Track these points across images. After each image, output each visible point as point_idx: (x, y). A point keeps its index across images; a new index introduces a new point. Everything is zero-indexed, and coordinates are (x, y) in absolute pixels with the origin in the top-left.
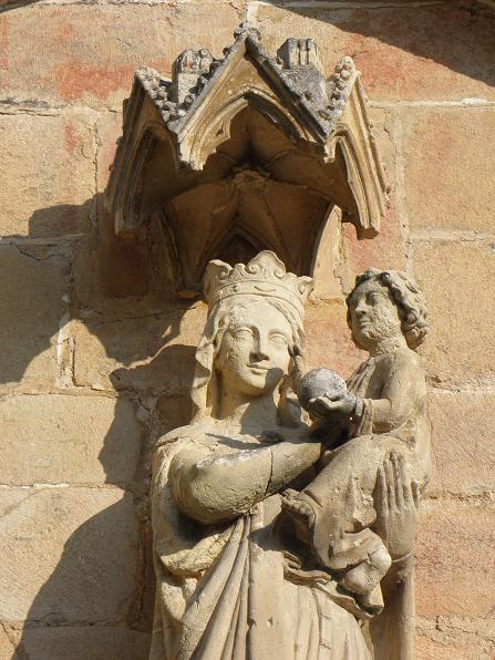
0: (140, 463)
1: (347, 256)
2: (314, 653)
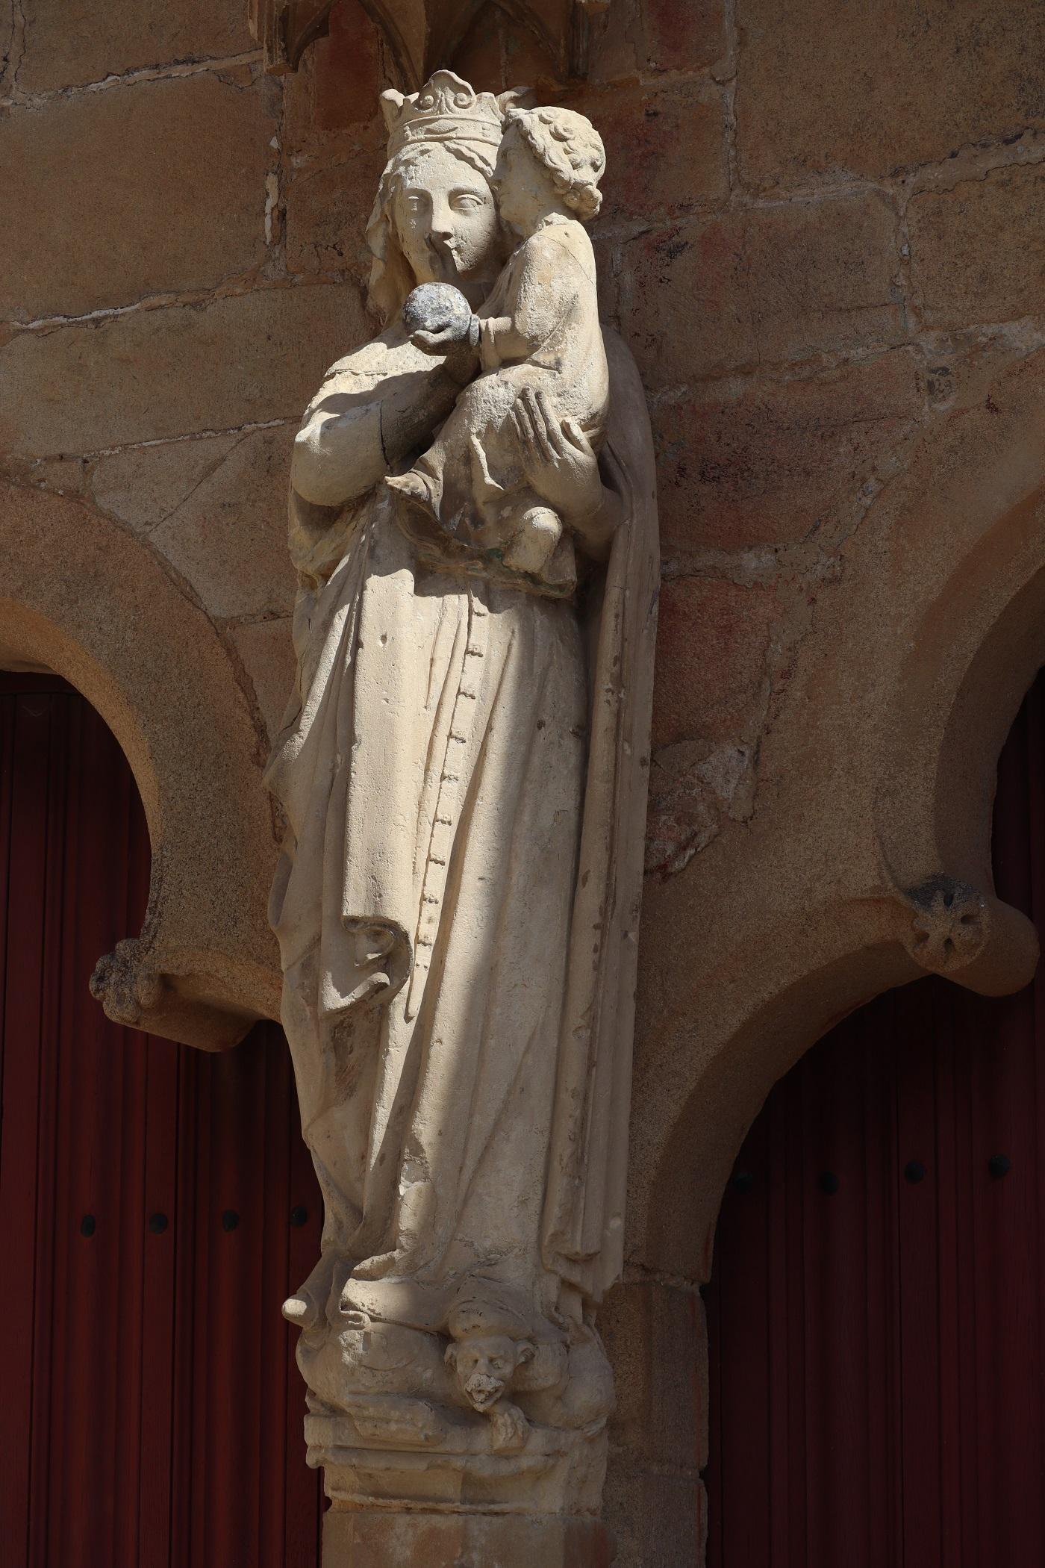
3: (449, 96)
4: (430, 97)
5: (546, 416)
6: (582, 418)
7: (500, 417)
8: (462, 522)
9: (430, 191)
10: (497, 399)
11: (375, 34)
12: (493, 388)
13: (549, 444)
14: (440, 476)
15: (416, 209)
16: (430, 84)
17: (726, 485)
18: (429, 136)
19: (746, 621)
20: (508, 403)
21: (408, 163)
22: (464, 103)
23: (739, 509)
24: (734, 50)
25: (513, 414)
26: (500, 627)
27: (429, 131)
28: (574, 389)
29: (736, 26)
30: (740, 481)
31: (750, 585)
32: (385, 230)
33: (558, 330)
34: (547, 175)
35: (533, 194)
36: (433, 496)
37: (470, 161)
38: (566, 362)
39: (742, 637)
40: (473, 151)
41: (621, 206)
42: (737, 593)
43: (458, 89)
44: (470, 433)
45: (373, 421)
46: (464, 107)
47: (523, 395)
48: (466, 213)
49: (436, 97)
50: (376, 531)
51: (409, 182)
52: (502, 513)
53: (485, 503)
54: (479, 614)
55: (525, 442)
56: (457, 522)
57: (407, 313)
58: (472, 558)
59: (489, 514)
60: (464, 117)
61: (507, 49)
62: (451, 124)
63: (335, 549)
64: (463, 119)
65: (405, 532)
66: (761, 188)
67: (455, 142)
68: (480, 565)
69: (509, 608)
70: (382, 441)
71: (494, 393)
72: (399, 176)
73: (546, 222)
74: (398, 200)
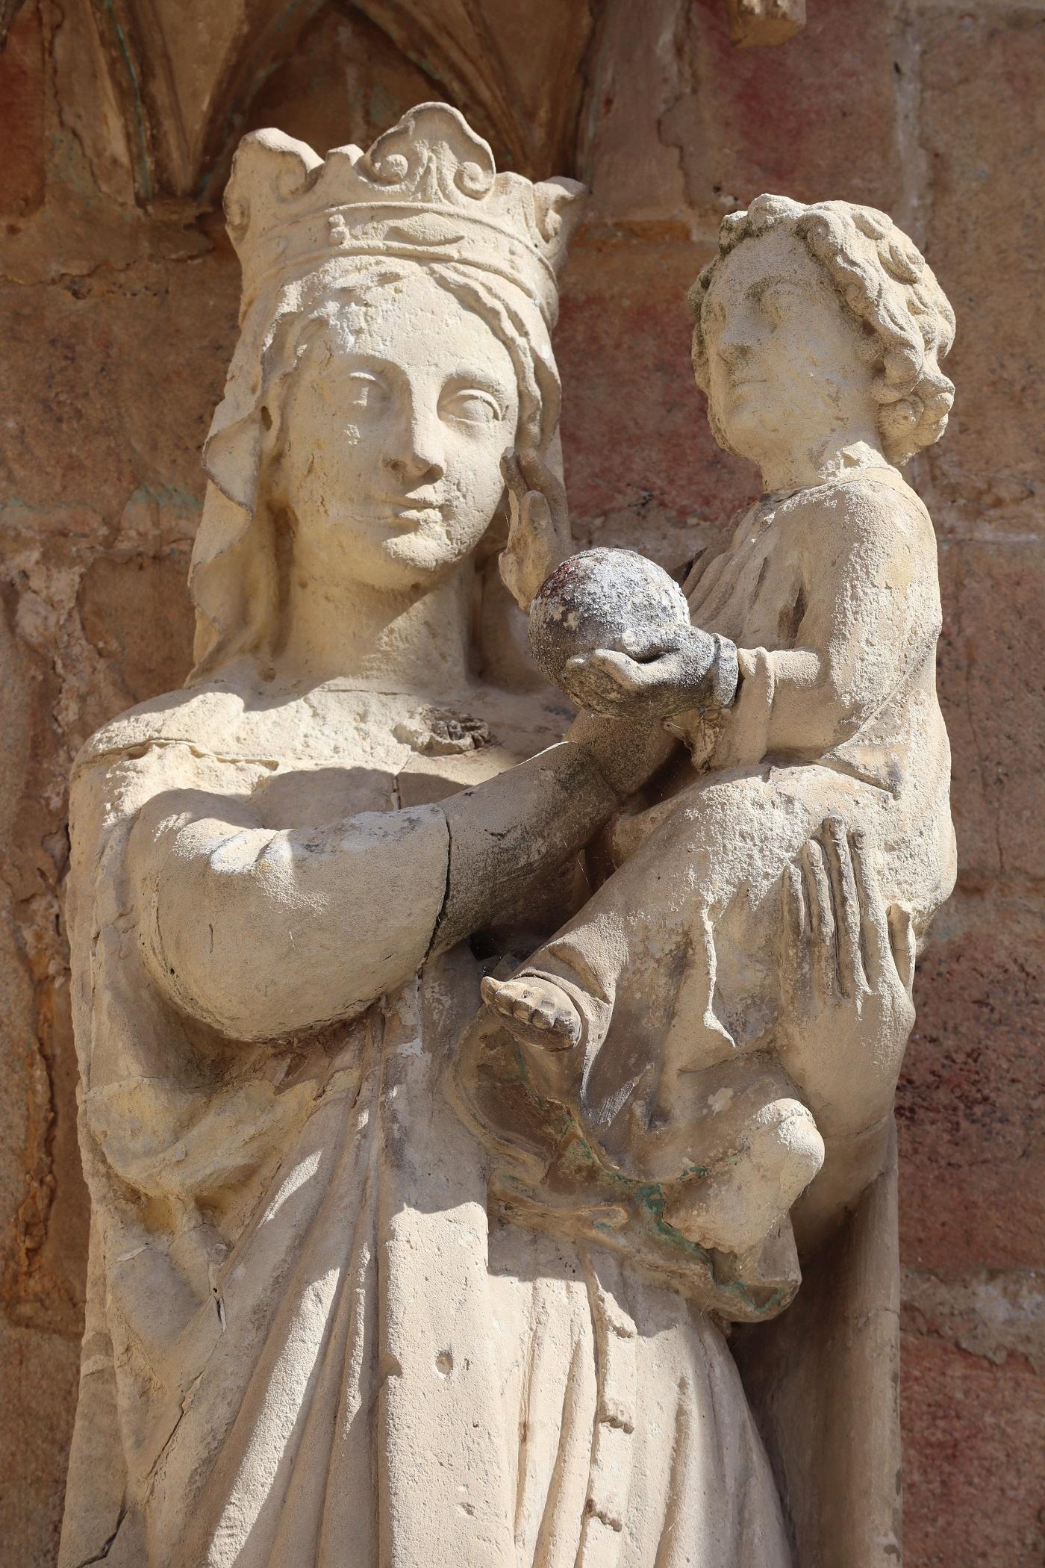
0: (33, 787)
1: (703, 70)
2: (581, 1445)
3: (447, 162)
4: (402, 159)
5: (865, 889)
6: (920, 908)
7: (766, 875)
8: (627, 1108)
9: (405, 367)
10: (769, 833)
11: (35, 24)
12: (762, 807)
13: (859, 954)
14: (611, 993)
15: (364, 402)
16: (406, 130)
17: (932, 1129)
18: (395, 244)
19: (992, 1438)
20: (790, 847)
21: (347, 295)
22: (477, 186)
23: (964, 1185)
24: (921, 197)
25: (796, 873)
26: (655, 1368)
27: (396, 234)
28: (920, 840)
29: (922, 145)
30: (964, 1124)
31: (1000, 1358)
32: (257, 441)
33: (894, 701)
34: (869, 352)
35: (833, 389)
36: (590, 1038)
37: (490, 316)
38: (906, 774)
39: (984, 1472)
40: (499, 298)
41: (656, 493)
42: (968, 1372)
43: (466, 150)
44: (700, 904)
45: (431, 849)
46: (475, 195)
47: (825, 832)
48: (470, 431)
49: (414, 159)
50: (401, 1106)
51: (351, 339)
52: (711, 1100)
53: (682, 1072)
54: (621, 1333)
55: (810, 943)
56: (618, 1107)
57: (570, 606)
58: (611, 1199)
59: (680, 1098)
60: (477, 218)
61: (367, 114)
62: (451, 228)
63: (253, 1138)
64: (475, 221)
65: (466, 1119)
66: (988, 499)
67: (456, 270)
68: (621, 1215)
69: (668, 1327)
70: (446, 897)
71: (764, 820)
72: (322, 322)
73: (847, 458)
74: (310, 375)
